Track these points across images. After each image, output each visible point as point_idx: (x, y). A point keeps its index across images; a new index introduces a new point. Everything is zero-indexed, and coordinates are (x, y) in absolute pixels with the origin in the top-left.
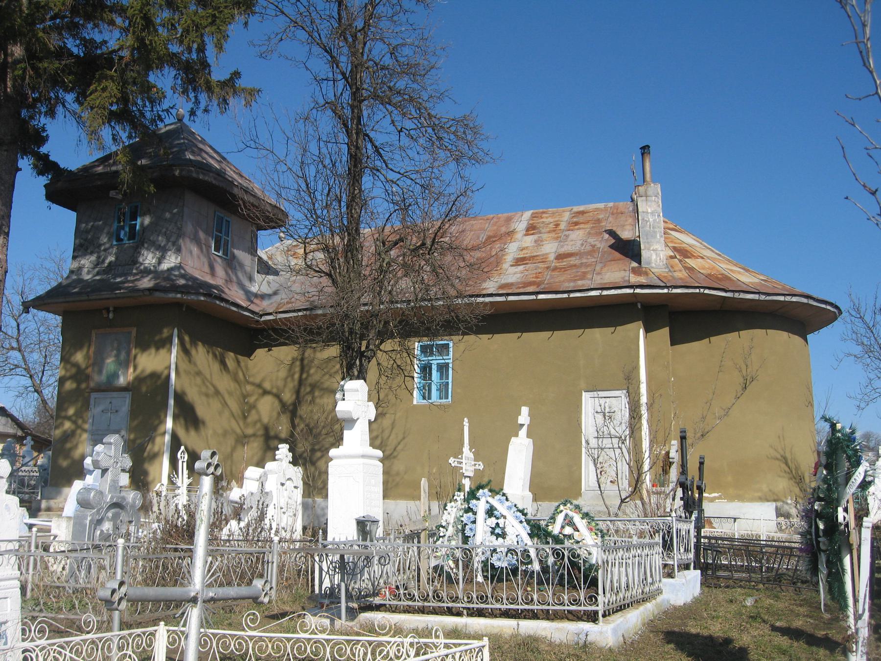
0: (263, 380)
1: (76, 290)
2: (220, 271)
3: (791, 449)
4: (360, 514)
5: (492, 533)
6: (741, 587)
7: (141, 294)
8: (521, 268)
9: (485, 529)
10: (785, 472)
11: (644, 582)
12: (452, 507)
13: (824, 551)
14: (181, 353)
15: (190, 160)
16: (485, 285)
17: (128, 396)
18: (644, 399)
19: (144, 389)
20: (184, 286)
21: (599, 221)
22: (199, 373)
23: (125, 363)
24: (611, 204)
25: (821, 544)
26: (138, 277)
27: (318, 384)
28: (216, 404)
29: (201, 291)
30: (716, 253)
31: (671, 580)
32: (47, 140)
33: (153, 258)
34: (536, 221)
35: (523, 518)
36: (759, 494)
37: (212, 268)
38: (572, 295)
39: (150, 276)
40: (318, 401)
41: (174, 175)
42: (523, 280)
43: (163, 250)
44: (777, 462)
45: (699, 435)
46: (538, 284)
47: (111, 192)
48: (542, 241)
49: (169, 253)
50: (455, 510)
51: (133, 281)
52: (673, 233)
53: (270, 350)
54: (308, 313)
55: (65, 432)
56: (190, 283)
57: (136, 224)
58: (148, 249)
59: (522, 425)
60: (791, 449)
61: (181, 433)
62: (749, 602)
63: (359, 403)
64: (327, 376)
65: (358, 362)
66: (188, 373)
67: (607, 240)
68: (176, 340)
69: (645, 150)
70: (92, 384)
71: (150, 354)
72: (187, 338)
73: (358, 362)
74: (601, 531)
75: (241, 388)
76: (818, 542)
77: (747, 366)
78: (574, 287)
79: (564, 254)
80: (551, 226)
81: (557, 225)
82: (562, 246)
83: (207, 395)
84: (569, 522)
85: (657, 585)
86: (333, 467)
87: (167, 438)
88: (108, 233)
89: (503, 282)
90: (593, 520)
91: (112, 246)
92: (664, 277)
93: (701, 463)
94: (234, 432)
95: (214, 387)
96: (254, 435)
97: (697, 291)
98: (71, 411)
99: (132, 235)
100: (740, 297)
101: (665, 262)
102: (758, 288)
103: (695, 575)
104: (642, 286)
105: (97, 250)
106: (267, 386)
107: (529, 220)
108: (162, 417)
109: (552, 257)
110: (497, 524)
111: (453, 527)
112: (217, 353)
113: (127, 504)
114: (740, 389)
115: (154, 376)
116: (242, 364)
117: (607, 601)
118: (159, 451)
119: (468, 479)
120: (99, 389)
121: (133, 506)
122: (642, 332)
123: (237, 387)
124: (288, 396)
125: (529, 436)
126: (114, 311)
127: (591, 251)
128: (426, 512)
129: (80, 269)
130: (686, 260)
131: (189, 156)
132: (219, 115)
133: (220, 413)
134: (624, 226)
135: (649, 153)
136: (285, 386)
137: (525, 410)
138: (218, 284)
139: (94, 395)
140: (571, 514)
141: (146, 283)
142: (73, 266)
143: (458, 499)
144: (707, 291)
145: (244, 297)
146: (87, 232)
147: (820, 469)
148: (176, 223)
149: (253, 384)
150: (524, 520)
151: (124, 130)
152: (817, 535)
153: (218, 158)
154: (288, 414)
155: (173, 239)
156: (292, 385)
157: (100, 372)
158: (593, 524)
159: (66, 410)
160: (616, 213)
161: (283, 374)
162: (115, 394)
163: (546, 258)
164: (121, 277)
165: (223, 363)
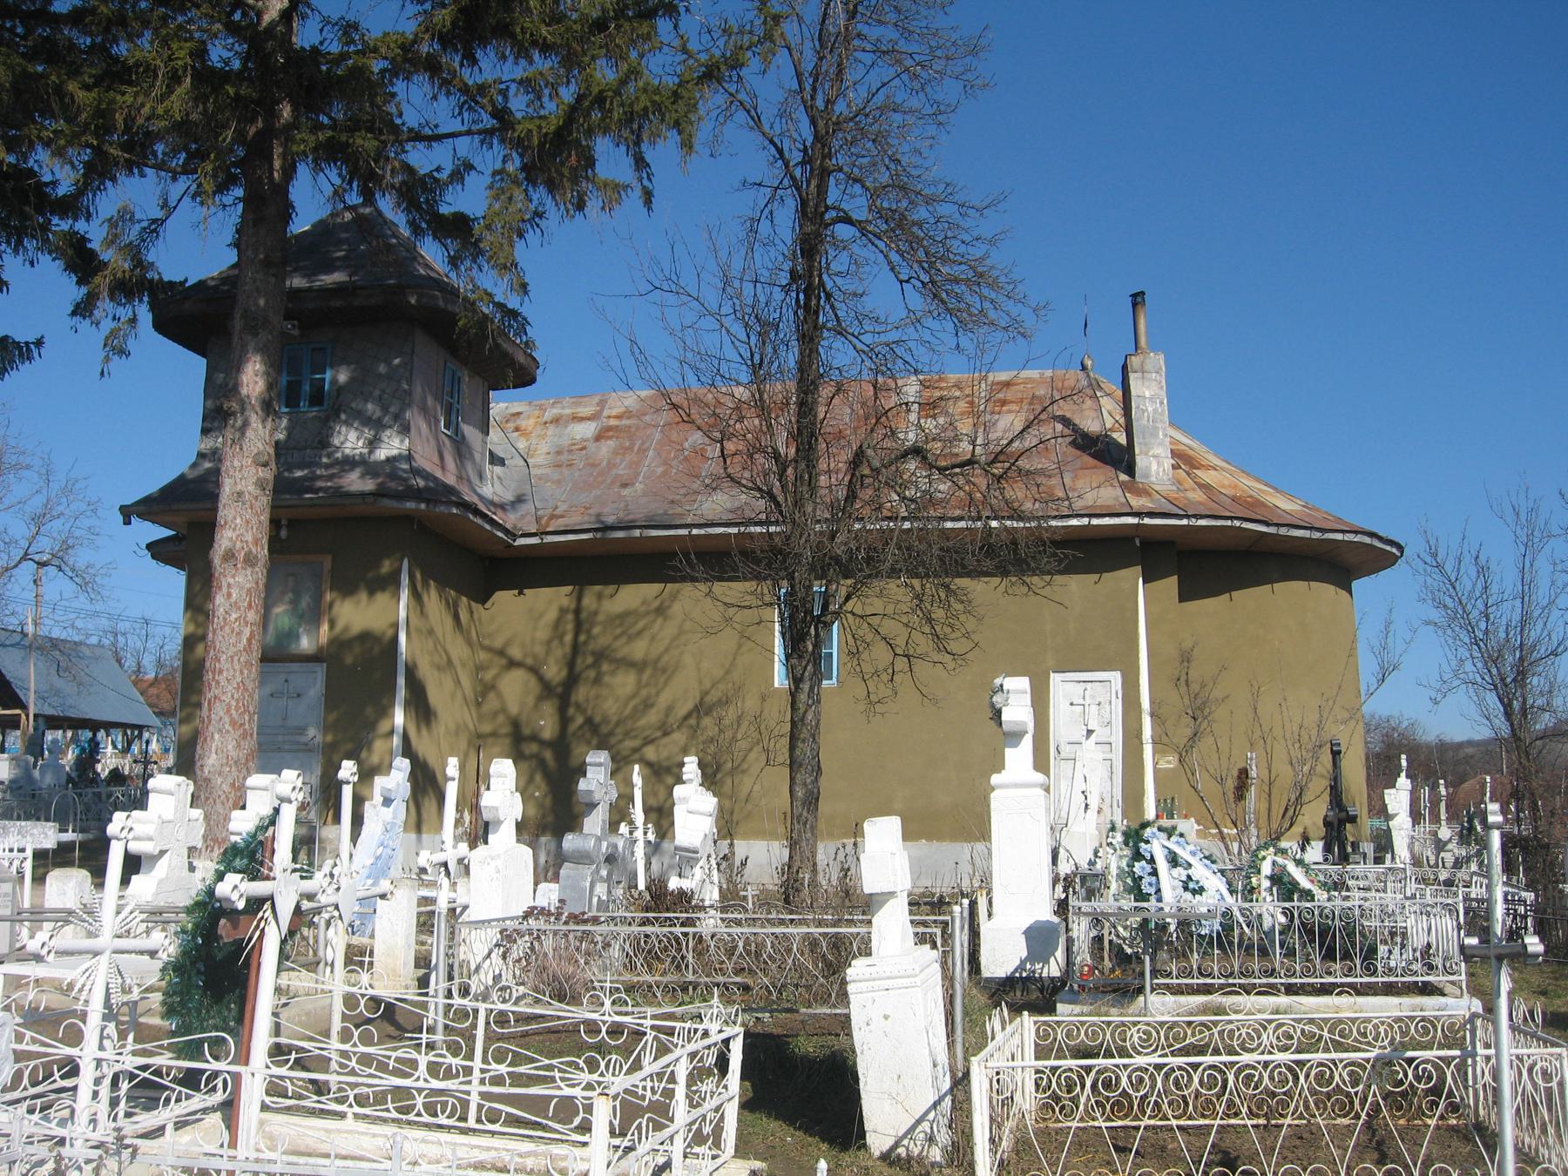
0: (508, 643)
5: (1186, 889)
19: (349, 660)
22: (431, 632)
23: (315, 614)
33: (358, 439)
40: (607, 679)
43: (378, 426)
49: (388, 432)
51: (330, 477)
53: (520, 593)
54: (599, 535)
58: (348, 424)
64: (624, 640)
66: (419, 631)
68: (405, 580)
69: (1137, 299)
71: (358, 602)
72: (418, 576)
83: (439, 668)
86: (996, 799)
96: (494, 734)
97: (1229, 523)
99: (317, 397)
104: (1151, 515)
106: (515, 652)
115: (366, 637)
116: (476, 616)
124: (554, 671)
126: (287, 526)
136: (547, 653)
142: (203, 446)
149: (489, 649)
154: (556, 702)
155: (392, 409)
156: (560, 652)
161: (543, 634)
162: (295, 666)
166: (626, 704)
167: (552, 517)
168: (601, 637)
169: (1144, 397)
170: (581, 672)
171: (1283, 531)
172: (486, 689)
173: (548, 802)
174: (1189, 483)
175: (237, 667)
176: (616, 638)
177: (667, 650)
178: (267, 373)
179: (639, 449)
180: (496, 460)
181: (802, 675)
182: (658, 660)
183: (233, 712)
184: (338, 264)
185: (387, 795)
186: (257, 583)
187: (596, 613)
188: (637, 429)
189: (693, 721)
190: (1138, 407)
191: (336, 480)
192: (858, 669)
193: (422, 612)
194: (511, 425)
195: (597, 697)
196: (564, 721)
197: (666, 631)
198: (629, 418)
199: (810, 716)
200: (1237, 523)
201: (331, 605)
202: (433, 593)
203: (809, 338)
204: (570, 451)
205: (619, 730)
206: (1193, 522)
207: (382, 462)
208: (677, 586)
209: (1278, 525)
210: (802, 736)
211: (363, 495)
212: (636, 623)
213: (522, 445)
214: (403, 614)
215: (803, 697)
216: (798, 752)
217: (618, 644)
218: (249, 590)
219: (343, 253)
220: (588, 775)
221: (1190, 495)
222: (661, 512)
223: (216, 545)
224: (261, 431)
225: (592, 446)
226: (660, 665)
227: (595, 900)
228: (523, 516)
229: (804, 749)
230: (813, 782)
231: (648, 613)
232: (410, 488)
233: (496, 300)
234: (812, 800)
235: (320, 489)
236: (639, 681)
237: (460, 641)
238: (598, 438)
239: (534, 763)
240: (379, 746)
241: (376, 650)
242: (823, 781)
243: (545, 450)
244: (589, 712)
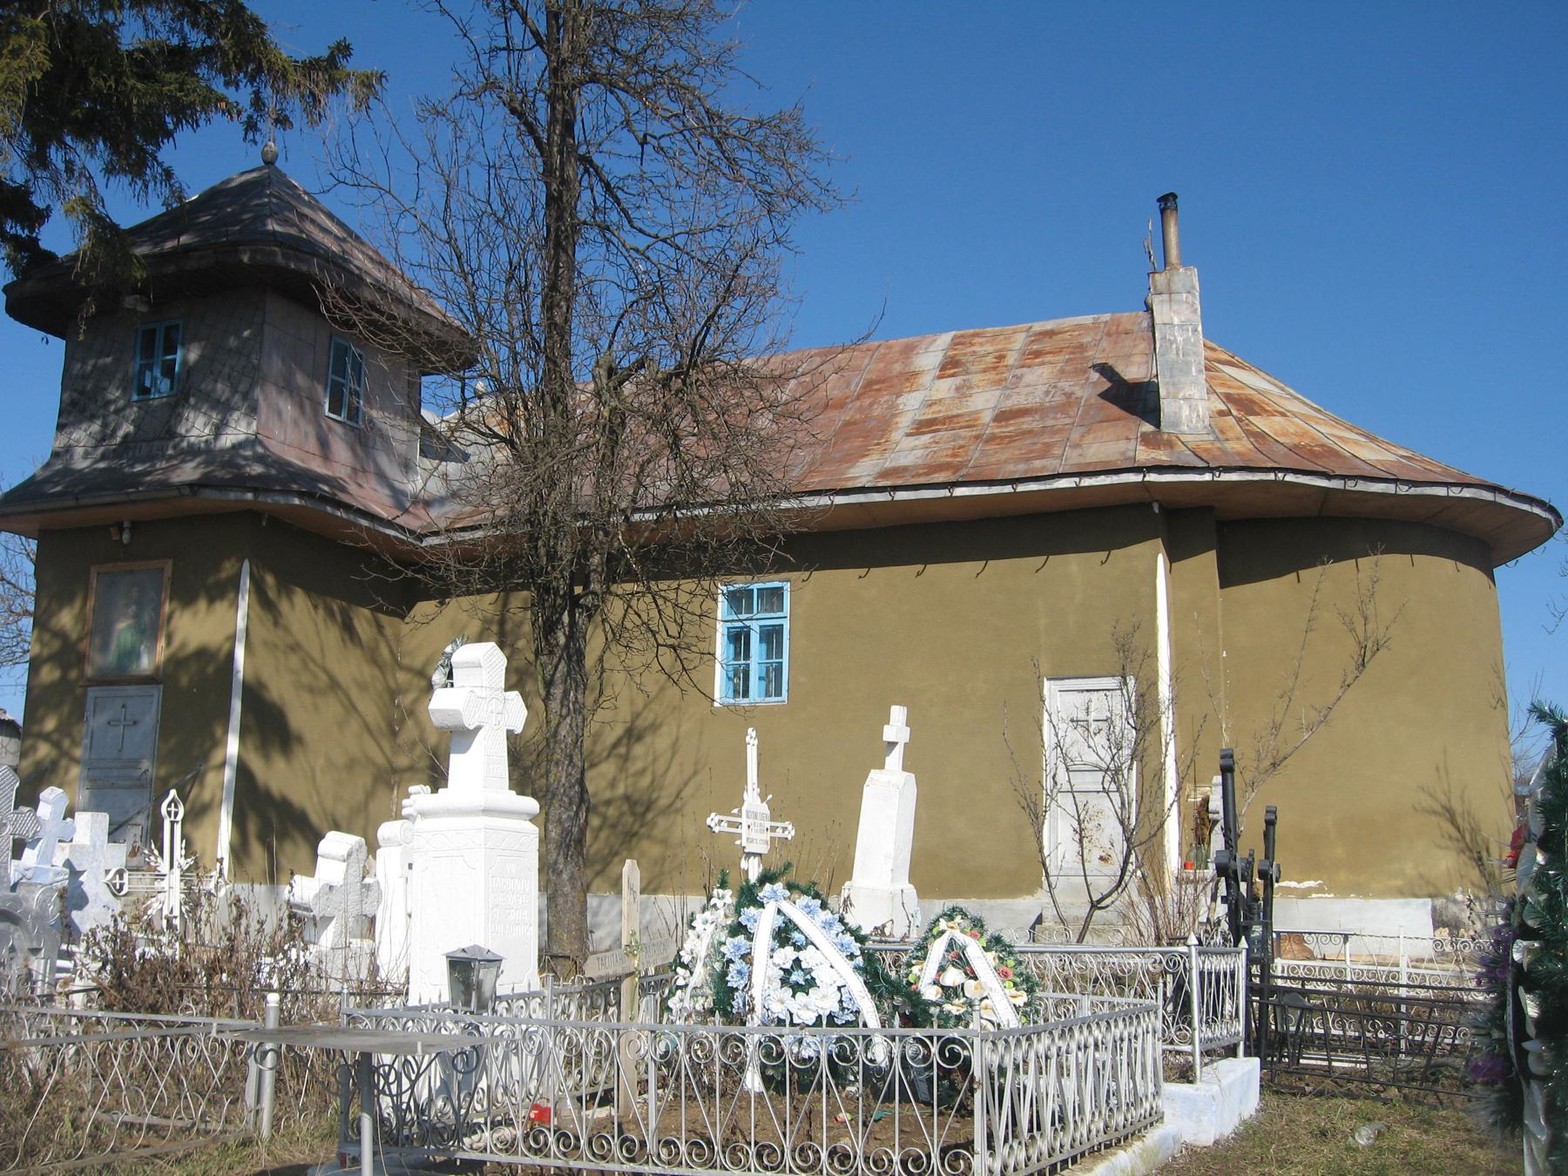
1: (58, 488)
2: (341, 451)
3: (1463, 792)
4: (458, 942)
5: (784, 982)
6: (1350, 1095)
8: (926, 439)
9: (770, 973)
10: (1450, 837)
11: (1113, 1101)
12: (706, 922)
13: (1543, 1079)
14: (258, 608)
15: (274, 232)
16: (853, 472)
17: (156, 693)
18: (1164, 690)
19: (184, 680)
20: (259, 477)
21: (1082, 348)
22: (295, 647)
23: (150, 630)
24: (1106, 317)
25: (1531, 1059)
26: (175, 462)
28: (332, 708)
29: (295, 487)
30: (1312, 407)
31: (1185, 1088)
32: (48, 216)
33: (205, 425)
34: (960, 350)
35: (855, 948)
36: (1399, 882)
37: (324, 444)
38: (1021, 488)
39: (198, 460)
41: (242, 261)
42: (928, 461)
43: (225, 408)
44: (1434, 818)
45: (1266, 763)
46: (957, 468)
48: (970, 388)
49: (236, 415)
50: (710, 928)
52: (1227, 369)
55: (38, 764)
56: (273, 472)
57: (175, 360)
58: (196, 408)
59: (892, 745)
60: (1463, 792)
61: (256, 764)
62: (1364, 1137)
63: (478, 692)
65: (566, 618)
67: (1095, 384)
68: (246, 583)
69: (1167, 202)
70: (89, 671)
71: (196, 613)
72: (270, 580)
73: (566, 618)
74: (1028, 979)
75: (385, 678)
76: (1523, 1054)
77: (1366, 619)
78: (1026, 471)
79: (1011, 411)
80: (990, 359)
81: (1001, 358)
82: (1008, 397)
83: (311, 690)
84: (958, 958)
85: (1147, 1105)
87: (229, 774)
89: (888, 465)
90: (1011, 953)
91: (129, 404)
92: (1206, 450)
93: (1270, 823)
94: (370, 761)
96: (411, 768)
97: (1271, 476)
98: (50, 724)
100: (1358, 488)
101: (1207, 423)
102: (1395, 472)
103: (1247, 1068)
105: (102, 411)
107: (948, 349)
108: (219, 732)
109: (987, 417)
110: (797, 962)
111: (705, 965)
112: (335, 608)
113: (26, 912)
114: (1351, 666)
116: (388, 631)
117: (997, 1167)
118: (212, 800)
119: (754, 861)
120: (107, 680)
121: (40, 917)
122: (1161, 560)
123: (377, 672)
125: (906, 767)
126: (131, 529)
127: (1063, 405)
128: (633, 934)
129: (68, 450)
130: (1251, 418)
131: (272, 226)
132: (306, 130)
133: (342, 725)
134: (1130, 355)
135: (1176, 209)
137: (898, 713)
138: (337, 475)
139: (93, 692)
140: (961, 938)
141: (189, 472)
142: (57, 444)
143: (720, 904)
144: (1290, 478)
145: (388, 501)
146: (85, 377)
147: (1527, 848)
148: (248, 356)
149: (409, 670)
150: (858, 953)
151: (92, 152)
152: (1521, 1035)
153: (335, 229)
155: (242, 387)
157: (105, 647)
158: (1011, 962)
159: (41, 721)
160: (1116, 333)
162: (132, 690)
163: (975, 420)
165: (348, 628)
169: (1172, 324)
189: (622, 750)
190: (1164, 338)
202: (300, 598)
207: (228, 449)
209: (1344, 477)
214: (241, 623)
241: (211, 669)
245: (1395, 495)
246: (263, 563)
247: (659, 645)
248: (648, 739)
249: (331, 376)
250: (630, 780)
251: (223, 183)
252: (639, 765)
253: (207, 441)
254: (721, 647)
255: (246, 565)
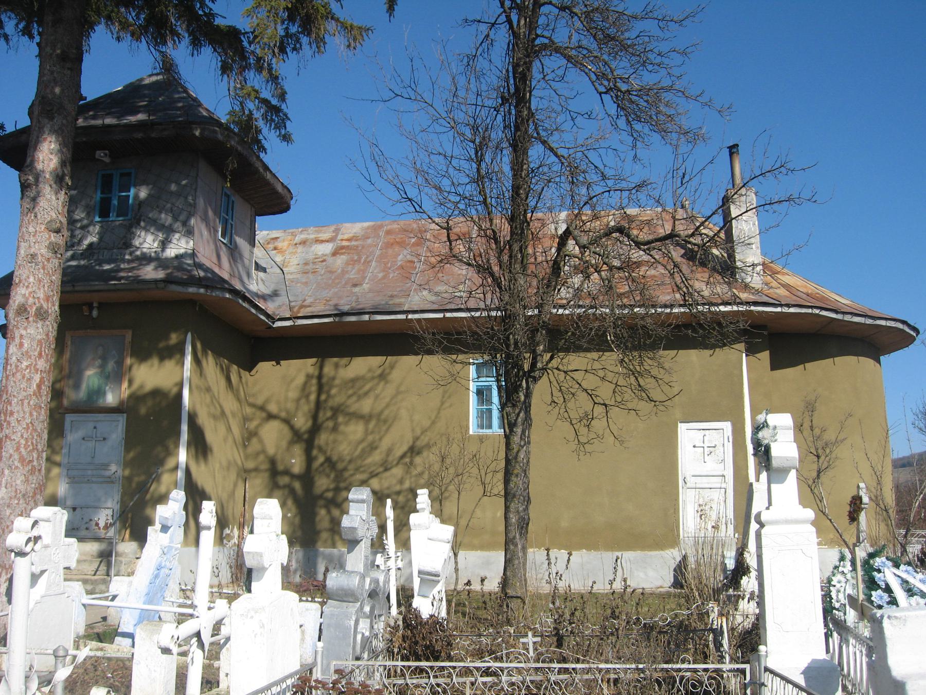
0: (267, 401)
7: (153, 286)
14: (194, 364)
19: (143, 411)
22: (208, 389)
23: (118, 375)
27: (342, 408)
40: (342, 428)
41: (195, 135)
43: (169, 231)
47: (98, 152)
49: (177, 236)
54: (337, 319)
57: (129, 196)
58: (147, 230)
64: (354, 398)
66: (198, 387)
68: (189, 349)
69: (733, 150)
71: (152, 366)
72: (199, 346)
83: (215, 417)
88: (87, 206)
91: (92, 223)
95: (221, 407)
96: (256, 470)
97: (810, 311)
104: (756, 303)
106: (273, 408)
108: (172, 446)
115: (156, 393)
116: (244, 380)
124: (302, 422)
126: (99, 308)
136: (297, 409)
139: (69, 418)
148: (186, 198)
149: (252, 405)
154: (303, 445)
155: (182, 217)
156: (306, 408)
157: (77, 386)
161: (293, 394)
162: (101, 416)
164: (109, 263)
166: (356, 449)
167: (302, 307)
168: (337, 397)
170: (323, 422)
171: (848, 318)
172: (251, 435)
173: (297, 520)
174: (774, 284)
175: (27, 409)
176: (350, 397)
177: (388, 406)
178: (60, 151)
179: (365, 261)
180: (258, 267)
181: (516, 420)
182: (382, 412)
183: (22, 450)
184: (142, 109)
185: (165, 523)
186: (47, 335)
187: (334, 378)
188: (363, 247)
189: (407, 460)
190: (737, 227)
191: (135, 272)
192: (566, 415)
193: (201, 375)
194: (271, 246)
195: (335, 441)
196: (309, 459)
197: (387, 391)
198: (357, 240)
199: (522, 455)
200: (817, 311)
201: (130, 368)
202: (211, 358)
203: (518, 147)
204: (314, 263)
205: (351, 467)
206: (785, 310)
207: (172, 258)
208: (395, 358)
210: (515, 472)
211: (156, 281)
212: (364, 386)
213: (279, 259)
215: (516, 439)
216: (512, 485)
217: (350, 401)
218: (40, 342)
219: (145, 103)
220: (352, 512)
221: (778, 291)
222: (383, 303)
223: (11, 301)
224: (54, 202)
225: (330, 260)
226: (383, 417)
227: (359, 637)
228: (280, 307)
229: (517, 482)
230: (524, 510)
231: (373, 378)
232: (193, 277)
233: (262, 96)
234: (524, 524)
235: (122, 278)
236: (366, 430)
237: (230, 396)
238: (335, 254)
239: (286, 491)
240: (166, 478)
241: (164, 403)
242: (531, 507)
243: (296, 262)
244: (328, 454)
245: (865, 324)
246: (198, 335)
247: (595, 403)
248: (425, 454)
249: (223, 214)
250: (413, 479)
251: (138, 80)
252: (419, 469)
253: (156, 252)
254: (473, 398)
255: (189, 336)
